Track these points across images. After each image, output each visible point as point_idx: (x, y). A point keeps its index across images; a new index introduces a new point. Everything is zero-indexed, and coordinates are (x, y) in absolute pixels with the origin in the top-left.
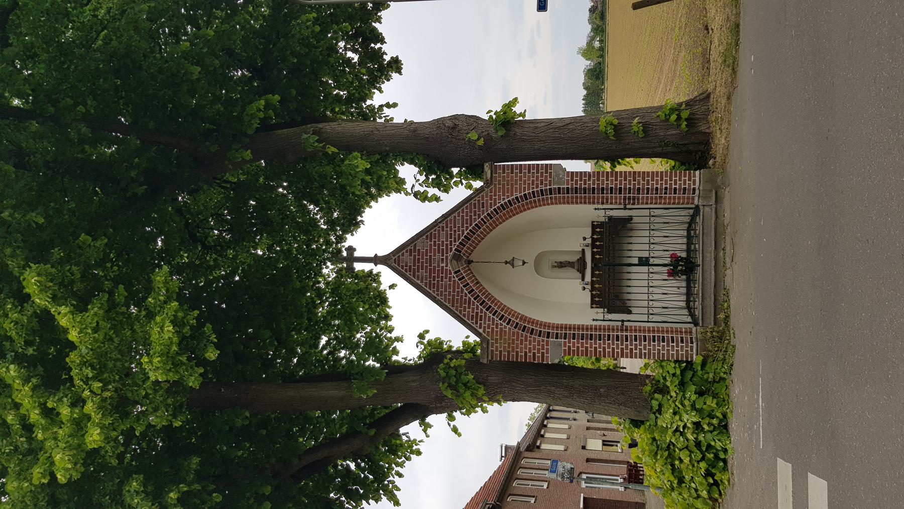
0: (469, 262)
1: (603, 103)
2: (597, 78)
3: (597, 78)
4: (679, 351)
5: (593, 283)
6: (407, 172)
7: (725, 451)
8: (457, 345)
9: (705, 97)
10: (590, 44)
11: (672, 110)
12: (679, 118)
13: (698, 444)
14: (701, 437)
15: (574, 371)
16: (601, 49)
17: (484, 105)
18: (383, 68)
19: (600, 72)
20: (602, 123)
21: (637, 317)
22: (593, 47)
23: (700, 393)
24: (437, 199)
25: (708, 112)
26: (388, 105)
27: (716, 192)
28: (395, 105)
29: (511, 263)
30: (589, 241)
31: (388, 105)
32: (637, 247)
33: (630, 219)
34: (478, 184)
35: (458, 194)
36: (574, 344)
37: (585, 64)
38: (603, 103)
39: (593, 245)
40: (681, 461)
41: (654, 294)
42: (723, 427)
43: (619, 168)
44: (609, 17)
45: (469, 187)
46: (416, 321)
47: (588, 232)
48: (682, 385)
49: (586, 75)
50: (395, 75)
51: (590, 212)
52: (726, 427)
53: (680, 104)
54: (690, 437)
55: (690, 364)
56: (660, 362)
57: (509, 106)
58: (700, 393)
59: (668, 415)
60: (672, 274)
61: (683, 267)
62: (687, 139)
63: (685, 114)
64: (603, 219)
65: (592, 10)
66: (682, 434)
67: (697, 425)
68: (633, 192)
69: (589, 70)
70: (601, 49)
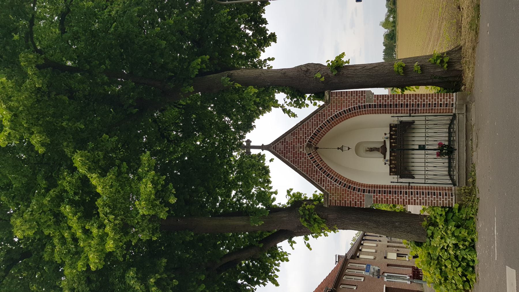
0: (317, 148)
1: (395, 54)
2: (392, 39)
3: (392, 39)
4: (445, 201)
6: (281, 97)
7: (473, 261)
8: (310, 196)
10: (387, 19)
11: (438, 57)
12: (442, 62)
13: (456, 257)
14: (458, 253)
16: (394, 22)
17: (325, 58)
19: (393, 35)
21: (418, 180)
22: (389, 21)
23: (458, 227)
24: (294, 115)
26: (269, 59)
27: (466, 105)
28: (273, 59)
29: (341, 149)
30: (388, 135)
32: (418, 138)
33: (413, 122)
34: (321, 103)
37: (384, 31)
38: (395, 54)
40: (446, 266)
41: (428, 167)
42: (472, 247)
45: (315, 104)
46: (286, 182)
48: (446, 221)
49: (385, 38)
50: (273, 43)
51: (388, 119)
52: (474, 247)
53: (443, 54)
54: (451, 252)
55: (451, 209)
58: (458, 227)
59: (437, 239)
60: (440, 154)
61: (446, 151)
63: (446, 59)
64: (396, 123)
66: (446, 250)
67: (456, 246)
68: (415, 106)
69: (386, 35)
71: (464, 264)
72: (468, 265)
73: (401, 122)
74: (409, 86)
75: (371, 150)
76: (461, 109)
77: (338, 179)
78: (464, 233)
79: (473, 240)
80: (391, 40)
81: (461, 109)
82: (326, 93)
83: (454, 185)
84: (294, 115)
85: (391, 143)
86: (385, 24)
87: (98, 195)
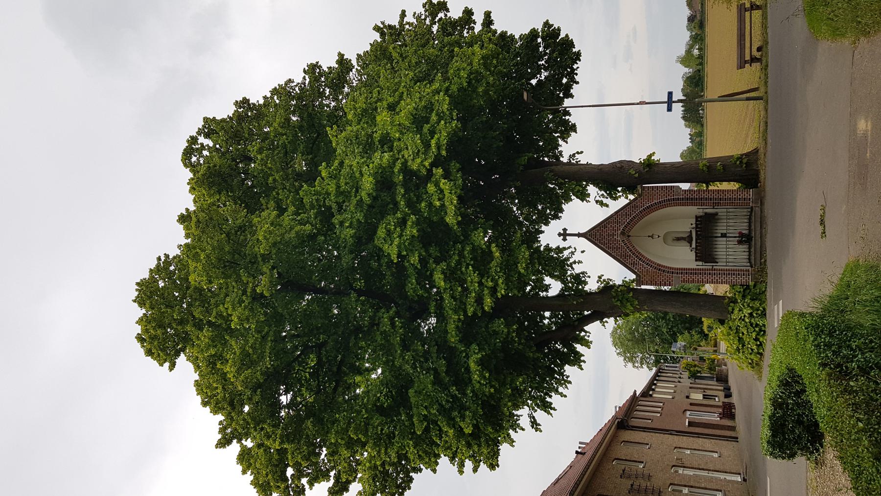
0: (629, 236)
1: (703, 110)
2: (697, 85)
3: (697, 85)
4: (742, 280)
5: (696, 249)
6: (592, 190)
7: (764, 326)
8: (618, 282)
9: (756, 151)
10: (689, 52)
11: (738, 159)
12: (741, 162)
13: (751, 325)
14: (752, 321)
15: (688, 294)
16: (701, 57)
17: (638, 157)
18: (569, 129)
19: (700, 79)
20: (701, 165)
21: (721, 265)
22: (692, 55)
23: (752, 300)
24: (607, 206)
25: (757, 160)
26: (578, 153)
27: (761, 199)
28: (582, 152)
29: (652, 237)
30: (694, 226)
31: (578, 153)
32: (721, 229)
33: (716, 214)
34: (631, 197)
35: (622, 202)
36: (686, 277)
37: (684, 70)
38: (703, 110)
39: (697, 227)
40: (743, 334)
41: (731, 254)
42: (764, 315)
43: (710, 188)
44: (708, 29)
45: (627, 198)
46: (598, 268)
47: (693, 221)
48: (744, 297)
49: (685, 82)
50: (573, 134)
51: (694, 210)
52: (765, 315)
53: (742, 155)
54: (747, 320)
55: (748, 286)
56: (733, 286)
57: (650, 156)
58: (752, 300)
59: (736, 312)
60: (740, 242)
61: (745, 239)
62: (746, 170)
63: (745, 161)
64: (701, 214)
65: (691, 19)
66: (743, 320)
67: (751, 315)
68: (720, 199)
69: (688, 78)
70: (701, 57)
71: (757, 329)
72: (761, 330)
73: (706, 213)
74: (713, 182)
75: (678, 239)
76: (756, 203)
77: (649, 263)
78: (757, 304)
79: (764, 309)
80: (698, 140)
81: (756, 203)
82: (639, 187)
83: (751, 267)
84: (607, 206)
85: (697, 232)
86: (685, 60)
87: (443, 273)
